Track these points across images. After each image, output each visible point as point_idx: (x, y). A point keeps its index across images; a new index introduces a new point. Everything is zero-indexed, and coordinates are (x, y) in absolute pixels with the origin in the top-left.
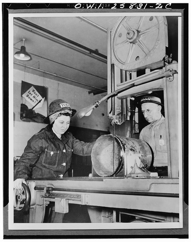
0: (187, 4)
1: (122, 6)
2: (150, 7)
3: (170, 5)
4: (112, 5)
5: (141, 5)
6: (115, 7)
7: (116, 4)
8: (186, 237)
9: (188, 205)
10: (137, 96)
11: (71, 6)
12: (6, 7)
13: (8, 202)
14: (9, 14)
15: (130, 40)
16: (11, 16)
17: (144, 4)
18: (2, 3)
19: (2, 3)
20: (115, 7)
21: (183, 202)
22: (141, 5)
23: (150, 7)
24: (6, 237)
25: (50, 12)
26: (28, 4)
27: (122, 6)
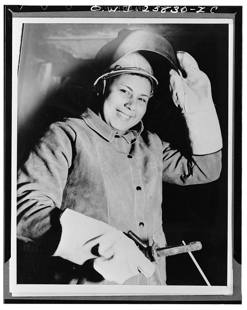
0: (241, 8)
1: (156, 9)
2: (191, 9)
3: (216, 9)
4: (197, 8)
5: (177, 8)
6: (147, 10)
7: (217, 7)
8: (239, 302)
9: (241, 264)
10: (170, 86)
11: (87, 8)
12: (10, 11)
13: (10, 257)
14: (13, 18)
15: (157, 256)
16: (17, 22)
17: (181, 7)
18: (4, 6)
19: (4, 6)
20: (147, 10)
21: (233, 259)
22: (177, 8)
23: (191, 9)
24: (7, 301)
25: (64, 16)
26: (69, 7)
27: (156, 9)
